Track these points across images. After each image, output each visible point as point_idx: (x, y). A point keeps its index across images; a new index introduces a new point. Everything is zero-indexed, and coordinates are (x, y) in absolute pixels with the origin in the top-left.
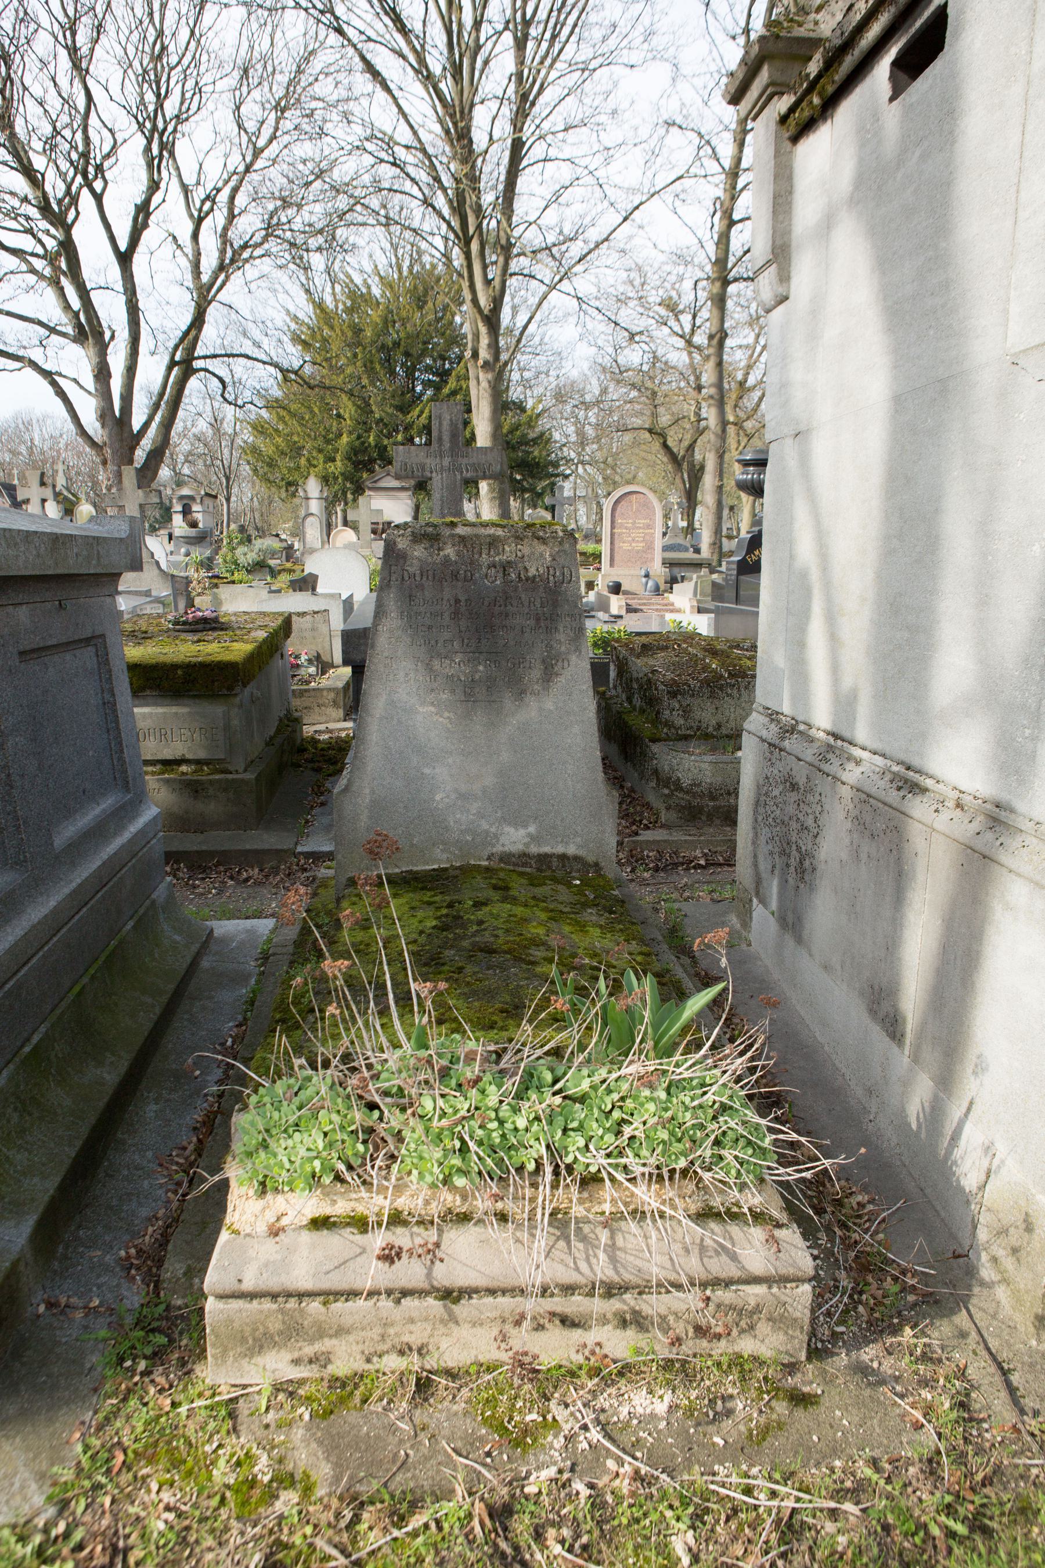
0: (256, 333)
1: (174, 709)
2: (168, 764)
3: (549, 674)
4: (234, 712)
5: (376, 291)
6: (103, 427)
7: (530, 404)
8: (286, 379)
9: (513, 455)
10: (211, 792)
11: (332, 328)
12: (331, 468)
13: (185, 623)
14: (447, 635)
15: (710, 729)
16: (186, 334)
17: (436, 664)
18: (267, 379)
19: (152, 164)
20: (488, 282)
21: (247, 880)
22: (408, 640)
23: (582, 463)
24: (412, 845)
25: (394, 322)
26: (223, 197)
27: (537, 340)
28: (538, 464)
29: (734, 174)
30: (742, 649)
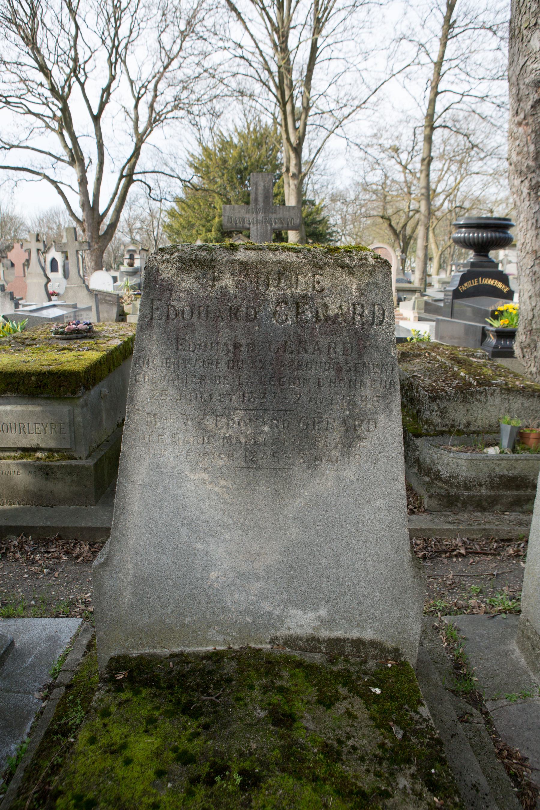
0: (172, 164)
1: (30, 408)
2: (27, 451)
3: (351, 437)
4: (78, 410)
5: (236, 140)
6: (83, 210)
7: (317, 203)
8: (186, 186)
9: (308, 230)
10: (59, 475)
11: (211, 160)
12: (209, 235)
13: (62, 333)
14: (223, 388)
15: (462, 427)
16: (129, 160)
17: (210, 423)
18: (178, 190)
19: (112, 65)
20: (296, 129)
21: (77, 557)
22: (176, 394)
23: (344, 235)
24: (183, 625)
25: (245, 156)
26: (151, 86)
27: (322, 167)
28: (321, 234)
29: (439, 64)
30: (476, 357)
